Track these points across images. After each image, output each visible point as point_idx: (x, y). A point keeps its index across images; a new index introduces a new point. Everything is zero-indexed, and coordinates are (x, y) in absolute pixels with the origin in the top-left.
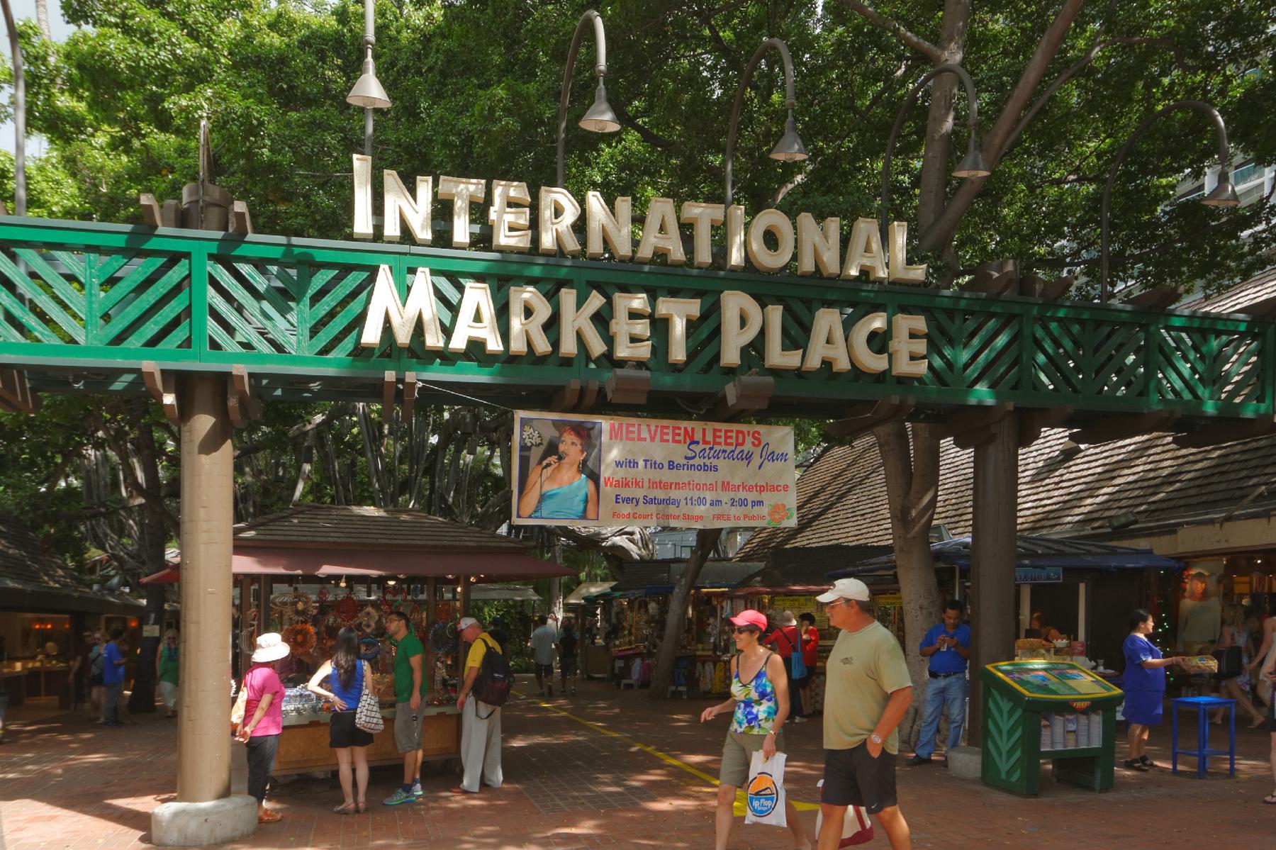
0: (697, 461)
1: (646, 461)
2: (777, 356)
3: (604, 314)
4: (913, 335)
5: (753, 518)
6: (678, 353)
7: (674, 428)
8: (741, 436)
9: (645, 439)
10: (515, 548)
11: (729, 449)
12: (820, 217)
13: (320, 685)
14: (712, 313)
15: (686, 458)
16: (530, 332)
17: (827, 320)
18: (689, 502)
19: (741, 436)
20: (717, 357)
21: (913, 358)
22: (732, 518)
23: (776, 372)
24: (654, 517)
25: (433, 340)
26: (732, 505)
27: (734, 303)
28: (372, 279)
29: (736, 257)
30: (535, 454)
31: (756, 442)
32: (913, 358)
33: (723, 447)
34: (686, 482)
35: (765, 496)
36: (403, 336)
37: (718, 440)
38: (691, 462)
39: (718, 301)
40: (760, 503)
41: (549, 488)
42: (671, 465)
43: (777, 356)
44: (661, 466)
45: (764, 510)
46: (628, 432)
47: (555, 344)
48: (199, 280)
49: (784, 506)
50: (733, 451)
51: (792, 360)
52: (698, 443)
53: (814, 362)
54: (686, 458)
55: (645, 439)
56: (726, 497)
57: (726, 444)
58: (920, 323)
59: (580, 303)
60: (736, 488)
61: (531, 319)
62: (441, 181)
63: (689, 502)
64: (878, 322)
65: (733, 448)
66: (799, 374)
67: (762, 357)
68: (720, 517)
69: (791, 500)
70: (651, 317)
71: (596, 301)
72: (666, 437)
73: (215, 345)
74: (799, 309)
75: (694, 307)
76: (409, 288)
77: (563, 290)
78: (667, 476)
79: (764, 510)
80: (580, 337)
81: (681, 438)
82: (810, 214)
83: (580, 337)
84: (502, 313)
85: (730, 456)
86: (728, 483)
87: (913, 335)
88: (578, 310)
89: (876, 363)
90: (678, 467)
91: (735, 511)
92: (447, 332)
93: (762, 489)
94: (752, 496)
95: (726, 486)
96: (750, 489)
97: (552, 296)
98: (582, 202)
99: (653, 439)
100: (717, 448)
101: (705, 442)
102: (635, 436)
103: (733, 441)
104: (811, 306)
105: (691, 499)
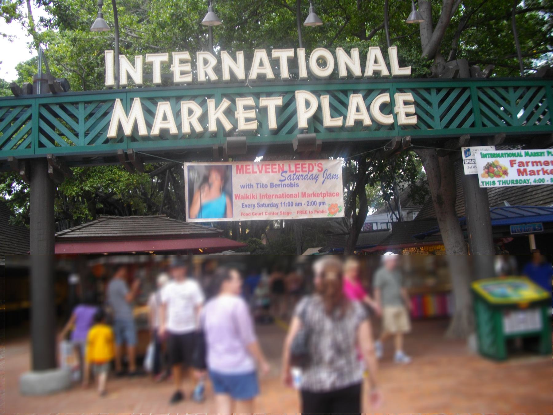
0: (287, 182)
1: (258, 184)
2: (329, 121)
4: (406, 103)
5: (320, 212)
6: (273, 124)
7: (302, 165)
8: (311, 167)
9: (256, 172)
10: (211, 234)
11: (305, 174)
14: (290, 102)
15: (280, 181)
16: (192, 123)
18: (283, 205)
19: (311, 167)
20: (296, 125)
21: (408, 115)
22: (308, 212)
23: (331, 129)
24: (264, 214)
25: (143, 131)
26: (308, 205)
27: (302, 96)
28: (112, 107)
29: (303, 73)
30: (196, 186)
31: (320, 169)
32: (408, 115)
33: (301, 173)
34: (271, 194)
35: (327, 199)
36: (128, 131)
37: (298, 170)
38: (283, 183)
40: (323, 203)
41: (204, 201)
42: (272, 185)
43: (329, 121)
44: (266, 186)
45: (326, 208)
46: (246, 169)
49: (337, 205)
50: (307, 175)
51: (338, 122)
52: (286, 172)
53: (350, 122)
54: (280, 181)
55: (256, 172)
56: (304, 201)
57: (303, 171)
58: (409, 97)
59: (217, 106)
60: (309, 196)
61: (192, 116)
62: (147, 57)
63: (283, 205)
64: (385, 98)
65: (307, 173)
66: (342, 128)
67: (321, 122)
68: (301, 212)
69: (340, 202)
70: (257, 107)
71: (225, 104)
72: (268, 170)
74: (341, 96)
75: (279, 101)
78: (270, 191)
79: (326, 208)
80: (218, 122)
81: (277, 170)
82: (341, 48)
83: (218, 122)
84: (177, 115)
85: (306, 178)
86: (305, 193)
87: (406, 103)
89: (388, 120)
90: (276, 186)
91: (310, 208)
92: (149, 126)
93: (325, 195)
94: (319, 200)
95: (304, 195)
96: (318, 195)
97: (203, 104)
99: (261, 172)
100: (298, 174)
101: (290, 171)
102: (251, 171)
103: (307, 169)
104: (346, 93)
105: (284, 203)
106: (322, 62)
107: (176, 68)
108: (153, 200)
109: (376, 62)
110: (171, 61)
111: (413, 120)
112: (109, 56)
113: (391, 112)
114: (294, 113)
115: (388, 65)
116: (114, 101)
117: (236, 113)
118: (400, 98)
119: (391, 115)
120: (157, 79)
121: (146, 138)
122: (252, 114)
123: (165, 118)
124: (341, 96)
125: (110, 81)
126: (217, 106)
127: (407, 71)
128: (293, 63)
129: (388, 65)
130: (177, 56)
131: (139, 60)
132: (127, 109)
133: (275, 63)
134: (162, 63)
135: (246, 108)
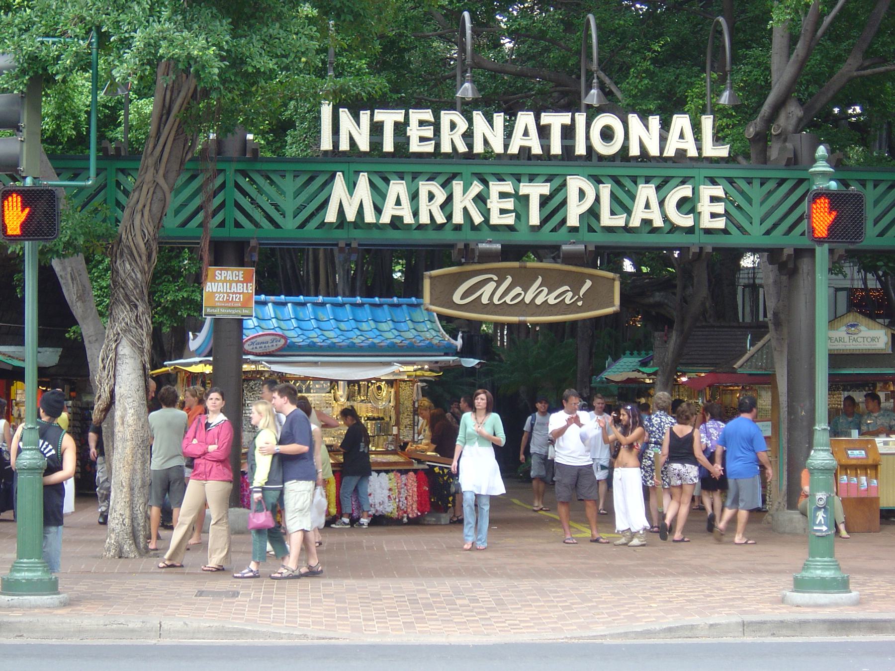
2: (607, 219)
3: (484, 194)
6: (535, 218)
12: (644, 117)
13: (456, 340)
17: (646, 192)
20: (564, 221)
23: (610, 230)
25: (370, 217)
27: (575, 183)
29: (580, 149)
36: (351, 216)
39: (565, 180)
43: (607, 219)
47: (449, 217)
48: (230, 185)
51: (619, 221)
53: (635, 222)
59: (465, 191)
64: (686, 191)
66: (626, 229)
67: (597, 217)
71: (476, 188)
73: (238, 225)
75: (545, 189)
76: (355, 185)
77: (454, 182)
82: (636, 115)
84: (414, 196)
87: (714, 199)
88: (464, 195)
89: (686, 221)
92: (378, 210)
98: (470, 121)
106: (607, 134)
107: (414, 132)
108: (397, 270)
109: (682, 136)
110: (407, 122)
111: (720, 223)
112: (326, 111)
113: (693, 211)
114: (564, 203)
115: (698, 139)
116: (333, 176)
117: (488, 201)
118: (707, 191)
119: (692, 215)
120: (388, 146)
121: (376, 226)
122: (509, 204)
123: (398, 202)
124: (628, 184)
125: (326, 144)
126: (465, 191)
127: (723, 151)
128: (568, 132)
129: (698, 139)
130: (416, 115)
131: (365, 116)
132: (351, 186)
133: (544, 132)
134: (396, 124)
135: (503, 195)
